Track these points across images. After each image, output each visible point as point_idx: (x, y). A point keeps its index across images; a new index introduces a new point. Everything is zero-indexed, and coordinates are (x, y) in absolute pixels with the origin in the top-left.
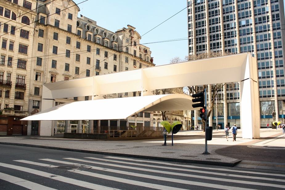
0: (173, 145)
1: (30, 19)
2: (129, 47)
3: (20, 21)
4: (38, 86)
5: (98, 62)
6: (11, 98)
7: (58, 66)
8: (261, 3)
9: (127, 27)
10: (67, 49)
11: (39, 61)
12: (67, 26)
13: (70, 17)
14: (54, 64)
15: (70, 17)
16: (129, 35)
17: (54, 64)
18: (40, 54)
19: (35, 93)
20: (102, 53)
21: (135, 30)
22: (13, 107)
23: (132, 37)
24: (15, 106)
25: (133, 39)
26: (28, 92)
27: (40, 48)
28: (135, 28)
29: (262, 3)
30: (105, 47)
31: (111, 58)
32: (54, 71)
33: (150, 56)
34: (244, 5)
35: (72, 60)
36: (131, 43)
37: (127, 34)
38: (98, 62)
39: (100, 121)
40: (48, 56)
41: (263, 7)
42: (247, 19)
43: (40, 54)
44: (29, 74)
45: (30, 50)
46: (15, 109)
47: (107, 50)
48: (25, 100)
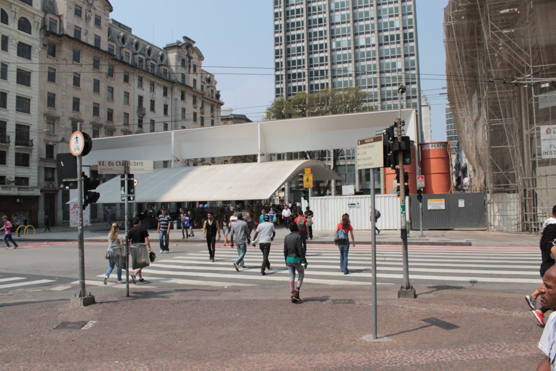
0: (171, 246)
1: (32, 22)
2: (187, 75)
3: (16, 27)
4: (51, 143)
5: (141, 99)
6: (9, 165)
7: (82, 107)
8: (388, 15)
9: (183, 41)
10: (96, 78)
11: (51, 100)
12: (93, 38)
13: (98, 22)
14: (76, 103)
15: (98, 22)
16: (186, 53)
17: (76, 103)
18: (51, 88)
19: (47, 156)
20: (104, 69)
21: (195, 45)
22: (14, 180)
23: (190, 58)
24: (16, 178)
25: (192, 61)
26: (36, 154)
27: (52, 77)
28: (194, 42)
29: (389, 13)
30: (144, 71)
31: (159, 92)
32: (76, 117)
33: (215, 88)
34: (389, 66)
35: (101, 98)
36: (190, 67)
37: (183, 51)
38: (141, 99)
39: (186, 204)
40: (64, 92)
41: (391, 19)
42: (368, 36)
43: (51, 88)
44: (34, 120)
45: (35, 79)
46: (16, 184)
47: (142, 75)
48: (32, 167)
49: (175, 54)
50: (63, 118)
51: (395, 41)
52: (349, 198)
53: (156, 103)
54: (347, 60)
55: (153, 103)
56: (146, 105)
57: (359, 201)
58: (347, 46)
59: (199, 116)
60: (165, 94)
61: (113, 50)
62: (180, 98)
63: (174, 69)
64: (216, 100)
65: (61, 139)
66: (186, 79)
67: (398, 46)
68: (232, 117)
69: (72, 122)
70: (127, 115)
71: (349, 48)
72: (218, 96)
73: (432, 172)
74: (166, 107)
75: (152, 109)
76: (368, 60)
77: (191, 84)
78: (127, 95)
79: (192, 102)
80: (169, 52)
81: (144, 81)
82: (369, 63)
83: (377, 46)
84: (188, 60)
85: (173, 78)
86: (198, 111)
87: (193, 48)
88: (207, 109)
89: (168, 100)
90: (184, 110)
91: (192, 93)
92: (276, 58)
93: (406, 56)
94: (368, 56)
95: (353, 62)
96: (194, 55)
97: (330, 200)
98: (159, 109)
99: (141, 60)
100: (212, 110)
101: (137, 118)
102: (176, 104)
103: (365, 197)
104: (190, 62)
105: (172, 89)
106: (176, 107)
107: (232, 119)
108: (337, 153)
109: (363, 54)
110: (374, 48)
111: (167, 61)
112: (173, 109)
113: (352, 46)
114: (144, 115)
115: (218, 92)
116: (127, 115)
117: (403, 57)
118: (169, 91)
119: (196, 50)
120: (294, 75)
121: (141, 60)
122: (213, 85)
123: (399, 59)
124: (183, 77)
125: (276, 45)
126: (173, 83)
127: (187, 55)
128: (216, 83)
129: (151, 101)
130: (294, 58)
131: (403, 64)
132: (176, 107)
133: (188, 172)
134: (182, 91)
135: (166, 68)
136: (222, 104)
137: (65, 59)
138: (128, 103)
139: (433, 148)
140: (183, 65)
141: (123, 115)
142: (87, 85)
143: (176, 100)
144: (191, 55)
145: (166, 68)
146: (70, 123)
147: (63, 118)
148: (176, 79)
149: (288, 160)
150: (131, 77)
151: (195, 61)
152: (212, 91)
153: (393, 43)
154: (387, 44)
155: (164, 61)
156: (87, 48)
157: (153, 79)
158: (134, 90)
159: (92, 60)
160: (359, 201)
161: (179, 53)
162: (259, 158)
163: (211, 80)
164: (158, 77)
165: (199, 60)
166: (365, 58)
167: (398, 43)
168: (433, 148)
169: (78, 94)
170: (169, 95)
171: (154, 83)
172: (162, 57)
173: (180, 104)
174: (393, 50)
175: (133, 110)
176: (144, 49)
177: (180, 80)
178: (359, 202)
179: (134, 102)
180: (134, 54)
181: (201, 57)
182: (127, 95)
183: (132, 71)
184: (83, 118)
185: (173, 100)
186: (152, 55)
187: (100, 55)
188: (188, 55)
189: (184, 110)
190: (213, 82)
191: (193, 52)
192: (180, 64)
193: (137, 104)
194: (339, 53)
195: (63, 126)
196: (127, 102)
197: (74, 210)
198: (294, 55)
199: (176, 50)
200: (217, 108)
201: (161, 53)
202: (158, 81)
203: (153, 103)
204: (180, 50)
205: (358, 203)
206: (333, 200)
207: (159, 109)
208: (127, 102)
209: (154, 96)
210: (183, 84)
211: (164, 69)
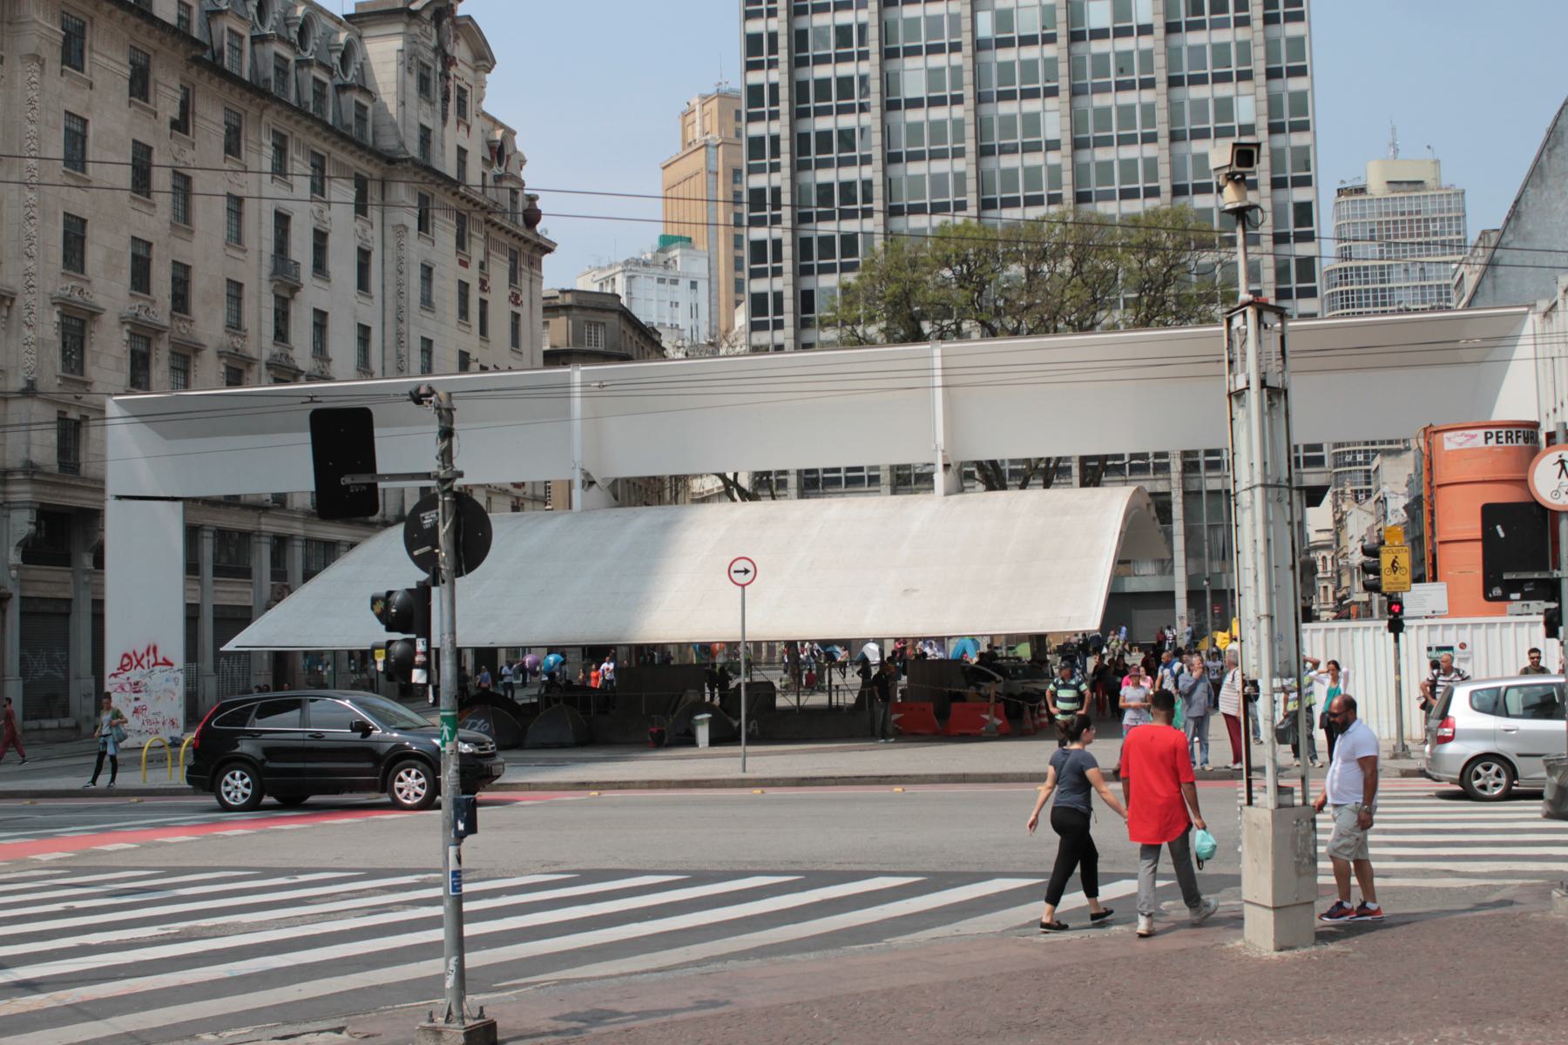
7: (94, 255)
16: (433, 43)
20: (167, 104)
23: (448, 61)
25: (453, 71)
33: (522, 184)
35: (154, 222)
36: (446, 99)
38: (282, 220)
49: (398, 43)
50: (29, 298)
51: (1231, 14)
52: (1419, 627)
53: (332, 241)
54: (1040, 85)
55: (320, 238)
56: (301, 250)
57: (1465, 636)
58: (1037, 31)
59: (475, 295)
60: (361, 208)
61: (188, 22)
62: (413, 223)
63: (392, 108)
64: (522, 232)
65: (22, 385)
66: (435, 146)
67: (1242, 34)
68: (569, 299)
69: (62, 315)
70: (235, 290)
71: (1050, 39)
72: (532, 217)
73: (1479, 544)
74: (364, 255)
75: (320, 267)
76: (1122, 86)
77: (451, 170)
78: (236, 204)
79: (452, 241)
80: (366, 32)
81: (291, 151)
82: (1128, 98)
83: (1159, 32)
84: (439, 69)
85: (388, 143)
86: (472, 275)
87: (456, 22)
88: (499, 271)
89: (369, 232)
90: (427, 272)
91: (452, 203)
92: (751, 66)
93: (1272, 74)
94: (1121, 71)
95: (1064, 94)
96: (461, 51)
97: (1359, 634)
98: (342, 264)
99: (281, 65)
100: (513, 277)
101: (269, 303)
102: (400, 246)
103: (1474, 625)
104: (445, 76)
105: (384, 183)
106: (400, 260)
107: (567, 308)
108: (1190, 464)
109: (1101, 61)
110: (1146, 42)
111: (363, 70)
112: (391, 267)
113: (1061, 31)
114: (295, 289)
115: (532, 199)
116: (235, 290)
117: (1260, 78)
118: (373, 192)
119: (469, 30)
120: (824, 138)
121: (281, 65)
122: (512, 170)
123: (1244, 86)
124: (425, 134)
125: (749, 16)
126: (390, 160)
127: (435, 50)
128: (523, 162)
129: (316, 231)
130: (822, 71)
131: (1264, 106)
132: (400, 260)
133: (667, 526)
134: (420, 195)
135: (364, 101)
136: (546, 248)
137: (36, 58)
138: (239, 240)
139: (1492, 442)
140: (424, 86)
141: (222, 289)
142: (110, 167)
143: (402, 229)
144: (449, 50)
145: (364, 101)
146: (56, 318)
147: (29, 298)
148: (402, 144)
149: (1083, 484)
150: (249, 135)
151: (462, 72)
152: (514, 192)
153: (1223, 24)
154: (1200, 26)
155: (352, 71)
156: (110, 14)
157: (322, 146)
158: (265, 195)
159: (127, 63)
160: (1465, 636)
161: (411, 40)
162: (939, 478)
163: (508, 151)
164: (342, 136)
165: (476, 70)
166: (1112, 79)
167: (1243, 22)
168: (1492, 442)
169: (80, 203)
170: (374, 213)
171: (322, 158)
172: (347, 54)
173: (416, 250)
174: (1221, 51)
175: (256, 273)
176: (286, 21)
177: (413, 149)
178: (1467, 641)
179: (259, 232)
180: (256, 40)
181: (484, 59)
182: (236, 204)
183: (253, 112)
184: (99, 300)
185: (389, 232)
186: (311, 46)
187: (153, 43)
188: (440, 50)
189: (427, 272)
190: (514, 161)
191: (456, 38)
192: (413, 82)
193: (269, 247)
194: (1005, 55)
195: (27, 332)
196: (236, 238)
197: (122, 678)
198: (823, 60)
199: (400, 28)
200: (531, 264)
201: (342, 37)
202: (338, 155)
203: (320, 238)
204: (415, 30)
205: (1463, 646)
206: (1370, 634)
207: (342, 264)
208: (236, 238)
209: (326, 214)
210: (424, 168)
211: (358, 103)
